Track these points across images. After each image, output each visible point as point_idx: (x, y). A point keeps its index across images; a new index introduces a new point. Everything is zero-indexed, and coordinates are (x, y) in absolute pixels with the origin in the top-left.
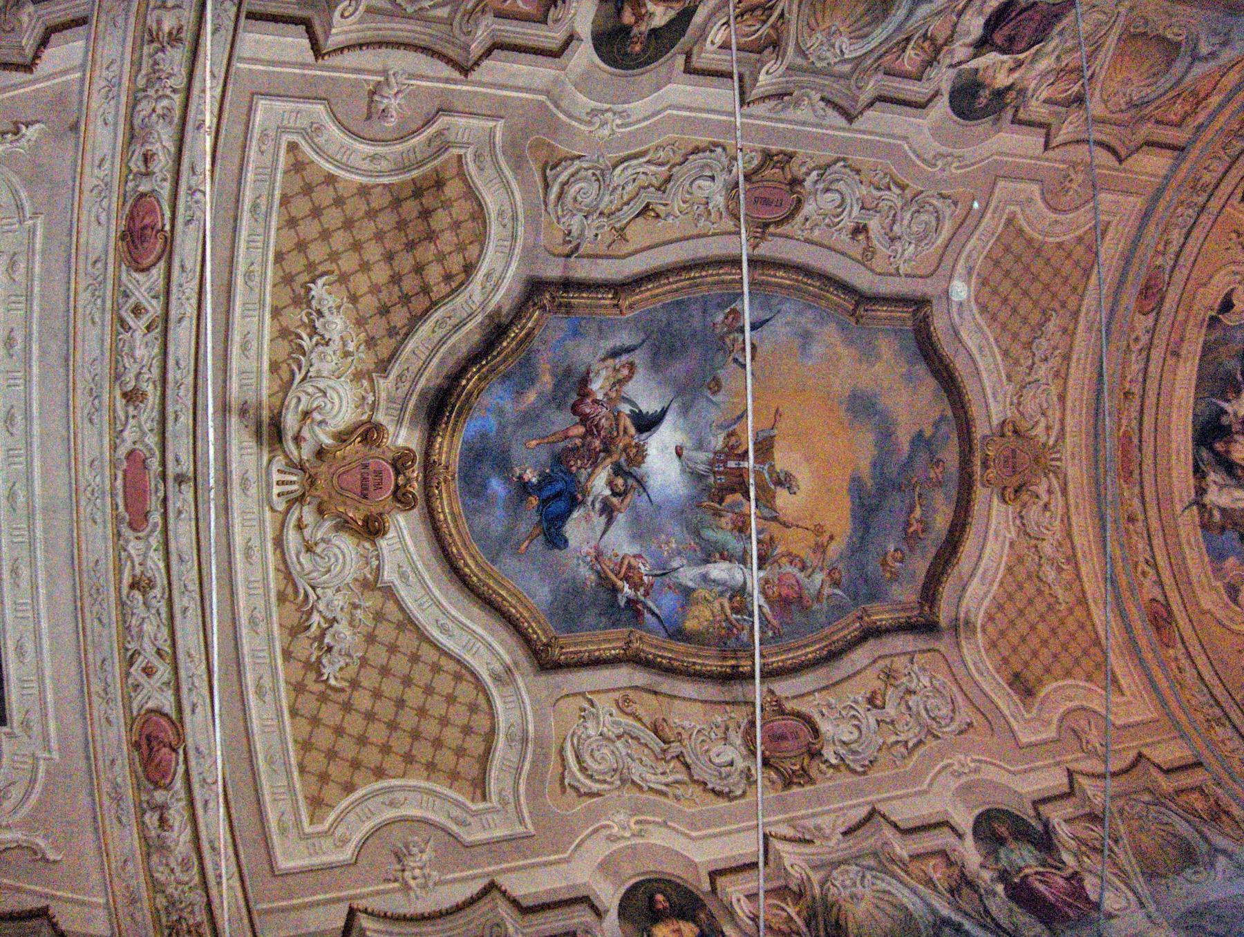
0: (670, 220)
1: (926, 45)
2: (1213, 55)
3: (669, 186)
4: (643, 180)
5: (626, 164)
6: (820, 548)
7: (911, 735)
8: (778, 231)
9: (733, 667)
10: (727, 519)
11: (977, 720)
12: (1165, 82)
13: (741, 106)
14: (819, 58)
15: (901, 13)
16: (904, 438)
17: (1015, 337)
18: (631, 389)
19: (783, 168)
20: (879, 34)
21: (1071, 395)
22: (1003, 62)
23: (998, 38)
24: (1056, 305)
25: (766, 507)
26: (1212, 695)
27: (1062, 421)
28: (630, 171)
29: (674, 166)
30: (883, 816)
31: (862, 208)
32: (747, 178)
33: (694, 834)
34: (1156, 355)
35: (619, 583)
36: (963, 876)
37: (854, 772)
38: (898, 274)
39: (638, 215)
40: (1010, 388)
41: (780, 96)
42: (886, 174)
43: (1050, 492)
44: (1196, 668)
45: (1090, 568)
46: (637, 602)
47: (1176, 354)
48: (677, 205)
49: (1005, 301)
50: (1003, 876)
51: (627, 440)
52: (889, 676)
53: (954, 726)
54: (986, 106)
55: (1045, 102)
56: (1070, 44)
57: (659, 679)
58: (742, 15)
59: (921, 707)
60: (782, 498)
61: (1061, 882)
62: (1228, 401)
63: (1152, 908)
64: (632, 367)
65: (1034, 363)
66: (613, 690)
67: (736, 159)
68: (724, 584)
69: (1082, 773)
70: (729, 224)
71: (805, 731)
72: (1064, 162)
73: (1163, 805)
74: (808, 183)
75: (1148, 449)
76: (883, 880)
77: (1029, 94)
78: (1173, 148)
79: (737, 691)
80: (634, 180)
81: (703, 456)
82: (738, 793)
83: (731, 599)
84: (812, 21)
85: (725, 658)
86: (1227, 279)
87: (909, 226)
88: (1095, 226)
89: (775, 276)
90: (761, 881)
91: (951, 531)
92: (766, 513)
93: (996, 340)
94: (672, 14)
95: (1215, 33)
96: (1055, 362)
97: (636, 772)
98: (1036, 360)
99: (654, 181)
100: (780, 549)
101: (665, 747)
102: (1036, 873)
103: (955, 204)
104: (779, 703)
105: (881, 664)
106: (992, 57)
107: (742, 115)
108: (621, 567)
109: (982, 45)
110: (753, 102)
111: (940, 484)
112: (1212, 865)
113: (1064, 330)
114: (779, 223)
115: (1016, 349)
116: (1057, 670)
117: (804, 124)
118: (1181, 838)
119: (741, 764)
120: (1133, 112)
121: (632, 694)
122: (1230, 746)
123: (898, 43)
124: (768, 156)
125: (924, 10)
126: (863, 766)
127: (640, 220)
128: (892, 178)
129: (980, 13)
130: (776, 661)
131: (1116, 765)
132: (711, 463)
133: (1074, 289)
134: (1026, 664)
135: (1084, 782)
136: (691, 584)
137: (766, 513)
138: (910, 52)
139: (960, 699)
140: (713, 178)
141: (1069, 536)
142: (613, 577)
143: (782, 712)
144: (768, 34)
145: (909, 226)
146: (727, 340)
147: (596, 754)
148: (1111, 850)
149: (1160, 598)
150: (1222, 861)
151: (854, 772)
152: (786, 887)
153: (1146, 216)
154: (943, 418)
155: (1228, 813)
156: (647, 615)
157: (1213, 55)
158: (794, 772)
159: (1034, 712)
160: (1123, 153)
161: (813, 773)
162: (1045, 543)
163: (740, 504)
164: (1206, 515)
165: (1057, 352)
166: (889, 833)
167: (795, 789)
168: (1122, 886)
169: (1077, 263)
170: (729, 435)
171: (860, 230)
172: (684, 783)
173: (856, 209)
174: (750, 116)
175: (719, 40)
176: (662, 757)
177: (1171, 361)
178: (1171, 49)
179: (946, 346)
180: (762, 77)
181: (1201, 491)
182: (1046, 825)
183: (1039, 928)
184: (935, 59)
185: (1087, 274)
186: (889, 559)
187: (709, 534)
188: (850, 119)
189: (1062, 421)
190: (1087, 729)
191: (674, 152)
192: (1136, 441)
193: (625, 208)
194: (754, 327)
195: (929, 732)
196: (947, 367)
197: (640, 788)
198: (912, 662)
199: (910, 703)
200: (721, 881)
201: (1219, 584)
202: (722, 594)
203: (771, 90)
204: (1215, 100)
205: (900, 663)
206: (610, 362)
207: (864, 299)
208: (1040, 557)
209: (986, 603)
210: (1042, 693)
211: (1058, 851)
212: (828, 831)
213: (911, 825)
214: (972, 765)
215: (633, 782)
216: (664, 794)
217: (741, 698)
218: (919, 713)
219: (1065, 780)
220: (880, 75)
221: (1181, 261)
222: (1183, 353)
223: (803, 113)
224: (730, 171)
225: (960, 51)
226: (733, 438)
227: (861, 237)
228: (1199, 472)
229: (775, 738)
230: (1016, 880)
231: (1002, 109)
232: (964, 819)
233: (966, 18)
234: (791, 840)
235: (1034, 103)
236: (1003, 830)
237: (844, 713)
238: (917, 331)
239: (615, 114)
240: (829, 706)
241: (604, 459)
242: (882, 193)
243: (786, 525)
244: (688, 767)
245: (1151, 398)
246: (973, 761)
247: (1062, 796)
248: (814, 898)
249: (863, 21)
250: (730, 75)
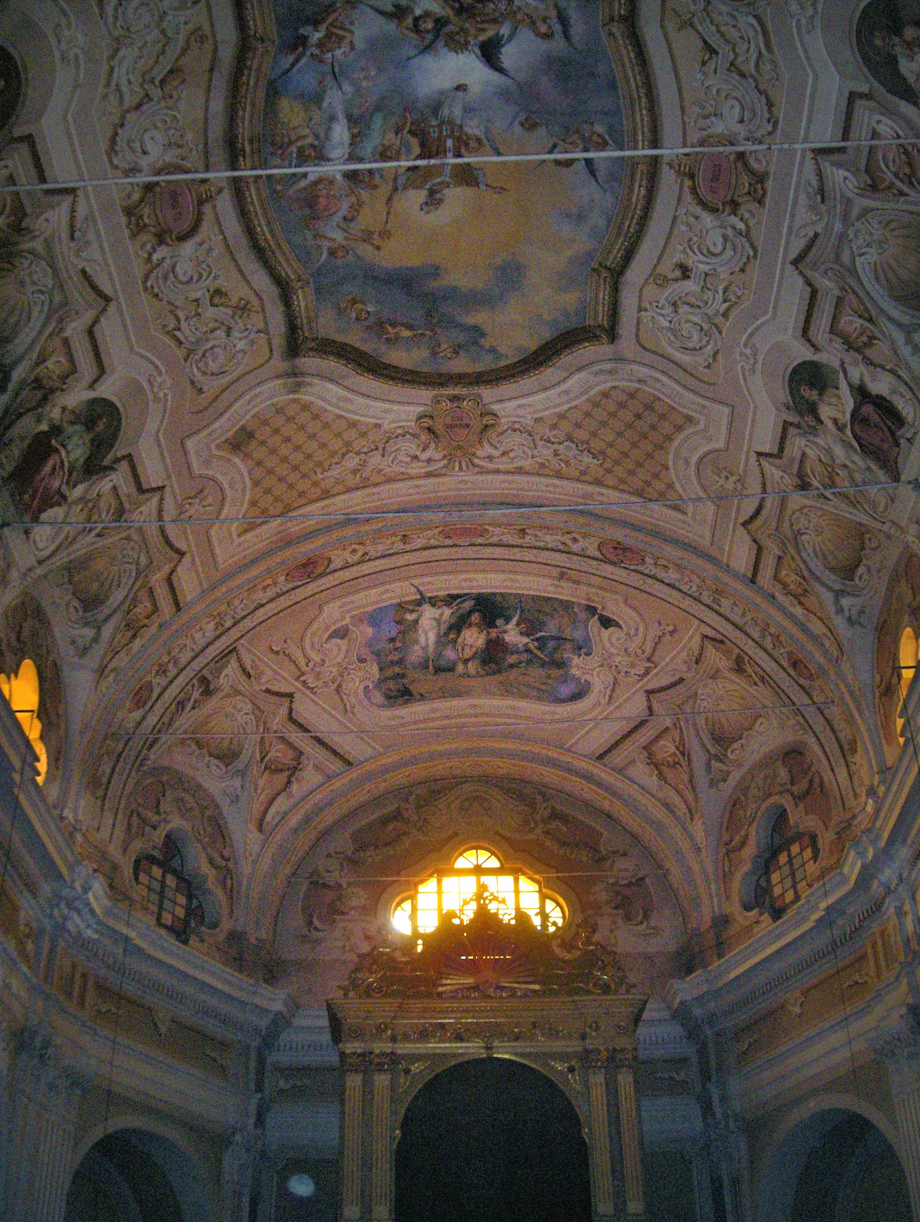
0: (699, 76)
1: (864, 338)
2: (840, 610)
3: (734, 75)
4: (741, 48)
5: (759, 29)
6: (367, 237)
7: (187, 333)
8: (686, 189)
9: (244, 150)
10: (393, 141)
11: (203, 400)
12: (817, 566)
13: (813, 151)
14: (858, 231)
15: (895, 314)
16: (478, 318)
17: (578, 425)
18: (526, 37)
19: (749, 193)
20: (877, 291)
21: (523, 479)
22: (844, 412)
23: (868, 409)
24: (608, 464)
25: (408, 180)
26: (244, 617)
27: (497, 472)
28: (751, 34)
29: (755, 80)
30: (104, 310)
31: (707, 275)
32: (741, 156)
33: (70, 119)
34: (559, 559)
35: (323, 27)
36: (53, 391)
37: (147, 277)
38: (640, 310)
39: (705, 42)
40: (528, 421)
41: (821, 191)
42: (739, 297)
43: (429, 461)
44: (268, 602)
45: (358, 500)
46: (305, 46)
47: (562, 576)
48: (714, 82)
49: (612, 415)
50: (56, 430)
51: (473, 31)
52: (243, 309)
53: (198, 376)
54: (803, 397)
55: (804, 454)
56: (858, 477)
57: (225, 72)
58: (906, 152)
59: (216, 343)
60: (418, 196)
61: (56, 484)
62: (518, 624)
63: (39, 571)
64: (548, 36)
65: (553, 443)
66: (212, 25)
67: (760, 143)
68: (327, 137)
69: (162, 499)
70: (694, 138)
71: (186, 226)
72: (745, 471)
73: (137, 578)
74: (734, 220)
75: (470, 552)
76: (40, 312)
77: (812, 438)
78: (755, 575)
79: (219, 155)
80: (742, 38)
81: (457, 112)
82: (116, 161)
83: (313, 146)
84: (893, 225)
85: (251, 142)
86: (632, 623)
87: (688, 321)
88: (681, 498)
89: (640, 186)
90: (28, 187)
91: (387, 366)
92: (402, 180)
93: (576, 407)
94: (911, 80)
95: (861, 612)
96: (555, 463)
97: (128, 53)
98: (555, 446)
99: (740, 59)
100: (365, 195)
101: (157, 82)
102: (62, 462)
103: (708, 367)
104: (210, 198)
105: (255, 301)
106: (849, 404)
107: (804, 150)
108: (341, 28)
109: (861, 393)
110: (817, 164)
111: (434, 354)
112: (86, 624)
113: (583, 473)
114: (694, 190)
115: (566, 426)
116: (258, 473)
117: (793, 216)
118: (107, 597)
119: (144, 162)
120: (789, 534)
121: (208, 46)
122: (198, 636)
123: (867, 310)
124: (761, 178)
125: (899, 336)
126: (152, 287)
127: (700, 44)
128: (736, 303)
129: (894, 392)
130: (252, 194)
131: (172, 532)
132: (450, 122)
133: (622, 481)
134: (263, 443)
135: (155, 501)
136: (325, 104)
137: (402, 180)
138: (858, 322)
139: (224, 380)
140: (741, 121)
141: (390, 480)
142: (330, 20)
143: (201, 203)
144: (885, 180)
145: (688, 321)
146: (576, 137)
147: (145, 8)
148: (91, 530)
149: (332, 567)
150: (90, 632)
151: (147, 277)
152: (25, 215)
153: (693, 549)
154: (499, 357)
155: (134, 636)
156: (291, 59)
157: (840, 610)
158: (141, 217)
159: (215, 452)
160: (752, 527)
161: (143, 237)
162: (379, 457)
163: (409, 151)
164: (411, 608)
165: (563, 465)
166: (89, 316)
167: (124, 220)
168: (57, 542)
169: (648, 484)
170: (479, 140)
171: (685, 272)
172: (121, 103)
173: (705, 268)
174: (803, 156)
175: (881, 128)
176: (146, 78)
177: (555, 572)
178: (848, 572)
179: (567, 359)
180: (842, 173)
181: (433, 602)
182: (111, 468)
183: (9, 467)
184: (850, 347)
185: (640, 493)
186: (359, 306)
187: (378, 121)
188: (796, 262)
189: (497, 472)
190: (204, 503)
191: (770, 80)
192: (480, 540)
193: (714, 28)
194: (589, 162)
195: (190, 352)
196: (549, 358)
197: (112, 57)
198: (258, 331)
199: (218, 332)
200: (24, 148)
201: (348, 620)
202: (317, 137)
203: (829, 183)
204: (798, 611)
205: (256, 320)
206: (553, 13)
207: (617, 274)
208: (365, 453)
209: (320, 403)
210: (237, 461)
211: (84, 481)
212: (84, 255)
213: (98, 335)
214: (161, 395)
215: (118, 50)
216: (108, 84)
217: (212, 160)
218: (208, 340)
219: (154, 485)
220: (837, 292)
221: (650, 581)
222: (563, 583)
223: (803, 215)
224: (747, 139)
225: (857, 372)
226: (476, 145)
227: (678, 273)
228: (451, 599)
229: (174, 195)
230: (53, 442)
231: (801, 414)
232: (105, 390)
233: (889, 378)
234: (72, 218)
235: (803, 442)
236: (101, 426)
237: (204, 266)
238: (584, 329)
239: (812, 17)
240: (210, 250)
241: (452, 8)
242: (721, 294)
243: (389, 200)
244: (138, 107)
245: (517, 554)
246: (166, 395)
247: (138, 483)
248: (17, 244)
249: (891, 276)
250: (845, 136)
